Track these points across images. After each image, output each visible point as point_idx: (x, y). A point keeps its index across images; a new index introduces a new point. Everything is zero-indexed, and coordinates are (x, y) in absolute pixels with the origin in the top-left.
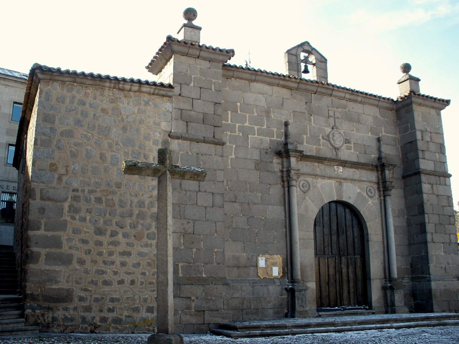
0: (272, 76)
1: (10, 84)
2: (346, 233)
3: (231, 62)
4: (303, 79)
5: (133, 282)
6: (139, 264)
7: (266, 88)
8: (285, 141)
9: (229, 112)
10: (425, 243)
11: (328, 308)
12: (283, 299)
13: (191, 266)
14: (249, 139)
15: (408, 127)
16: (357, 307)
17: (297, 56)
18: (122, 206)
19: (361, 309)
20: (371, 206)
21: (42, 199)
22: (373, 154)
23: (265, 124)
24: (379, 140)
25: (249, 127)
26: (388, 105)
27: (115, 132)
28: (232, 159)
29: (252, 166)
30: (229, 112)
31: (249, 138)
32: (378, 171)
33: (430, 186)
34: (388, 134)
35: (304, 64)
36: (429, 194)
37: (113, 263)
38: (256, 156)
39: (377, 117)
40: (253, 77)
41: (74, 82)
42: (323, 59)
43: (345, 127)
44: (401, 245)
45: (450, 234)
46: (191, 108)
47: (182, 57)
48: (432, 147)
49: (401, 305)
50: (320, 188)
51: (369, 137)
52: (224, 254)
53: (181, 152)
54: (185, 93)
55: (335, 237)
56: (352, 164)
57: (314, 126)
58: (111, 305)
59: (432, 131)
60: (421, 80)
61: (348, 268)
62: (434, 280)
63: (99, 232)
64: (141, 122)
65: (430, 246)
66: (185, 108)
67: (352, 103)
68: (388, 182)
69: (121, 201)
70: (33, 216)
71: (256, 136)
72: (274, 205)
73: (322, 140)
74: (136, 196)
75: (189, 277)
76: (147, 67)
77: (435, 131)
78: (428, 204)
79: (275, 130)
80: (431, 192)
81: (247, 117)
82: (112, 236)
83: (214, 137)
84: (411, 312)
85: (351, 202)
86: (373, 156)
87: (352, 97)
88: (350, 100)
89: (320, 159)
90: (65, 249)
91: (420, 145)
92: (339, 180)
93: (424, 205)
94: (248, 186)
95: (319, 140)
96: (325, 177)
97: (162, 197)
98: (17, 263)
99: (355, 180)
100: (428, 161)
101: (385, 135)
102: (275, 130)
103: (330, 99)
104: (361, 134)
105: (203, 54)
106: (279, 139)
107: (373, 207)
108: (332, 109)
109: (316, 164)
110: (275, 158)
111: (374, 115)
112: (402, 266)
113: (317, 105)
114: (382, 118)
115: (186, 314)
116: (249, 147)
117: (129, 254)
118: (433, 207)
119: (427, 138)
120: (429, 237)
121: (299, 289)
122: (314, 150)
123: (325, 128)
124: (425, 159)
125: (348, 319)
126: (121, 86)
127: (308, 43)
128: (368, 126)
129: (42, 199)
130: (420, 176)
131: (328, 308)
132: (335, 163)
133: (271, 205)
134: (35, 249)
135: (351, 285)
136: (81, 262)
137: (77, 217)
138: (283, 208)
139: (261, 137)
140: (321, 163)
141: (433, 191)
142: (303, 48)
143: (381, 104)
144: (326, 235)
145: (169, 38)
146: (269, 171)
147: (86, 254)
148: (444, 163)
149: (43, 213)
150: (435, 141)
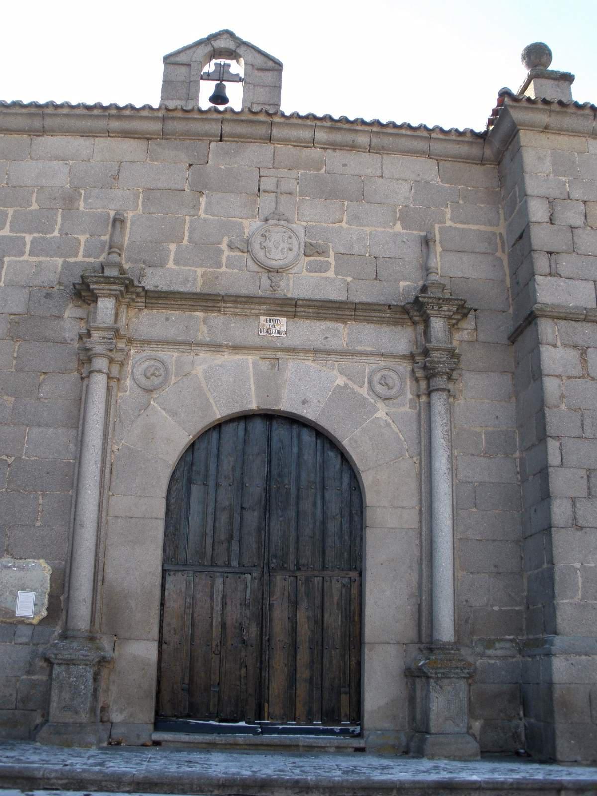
0: (85, 112)
2: (297, 504)
11: (211, 722)
14: (5, 267)
16: (318, 725)
19: (332, 732)
20: (382, 423)
22: (405, 279)
23: (57, 227)
24: (427, 242)
25: (11, 238)
26: (464, 149)
31: (6, 263)
32: (415, 324)
34: (464, 223)
36: (569, 377)
38: (45, 294)
40: (37, 123)
43: (310, 215)
44: (494, 541)
49: (457, 729)
50: (201, 375)
51: (395, 235)
55: (256, 514)
56: (319, 308)
57: (205, 220)
60: (521, 50)
61: (295, 605)
62: (566, 652)
65: (560, 538)
67: (342, 152)
68: (438, 350)
72: (47, 426)
73: (227, 252)
78: (563, 407)
79: (82, 238)
81: (10, 216)
85: (310, 413)
86: (403, 284)
87: (338, 137)
88: (334, 146)
89: (207, 300)
93: (547, 411)
95: (221, 252)
96: (221, 346)
99: (329, 352)
100: (570, 281)
101: (456, 228)
102: (82, 238)
103: (269, 148)
104: (367, 229)
106: (92, 260)
107: (393, 426)
108: (272, 172)
109: (200, 315)
110: (70, 306)
111: (418, 179)
112: (492, 606)
113: (223, 167)
114: (447, 185)
118: (582, 416)
120: (560, 511)
121: (60, 657)
122: (199, 278)
123: (244, 221)
124: (561, 276)
128: (395, 206)
131: (211, 722)
132: (257, 307)
133: (39, 425)
135: (303, 656)
139: (41, 259)
140: (213, 311)
142: (213, 46)
143: (437, 147)
144: (224, 509)
146: (47, 340)
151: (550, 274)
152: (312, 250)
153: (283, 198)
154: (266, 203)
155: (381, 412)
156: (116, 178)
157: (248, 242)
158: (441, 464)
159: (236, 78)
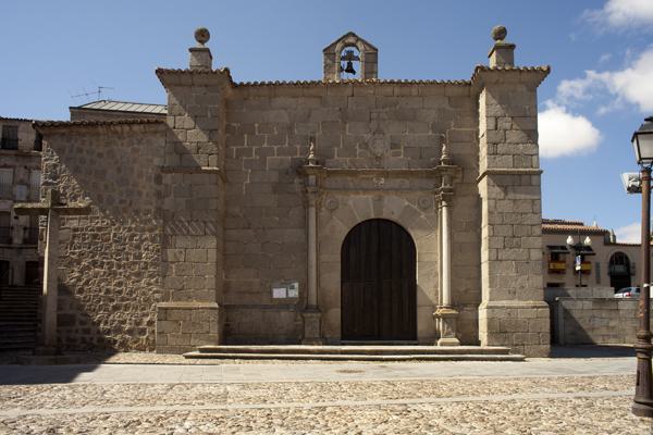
9: (246, 136)
38: (274, 177)
64: (135, 161)
75: (611, 319)
79: (298, 147)
85: (394, 218)
102: (298, 147)
104: (417, 135)
152: (394, 146)
154: (373, 125)
156: (309, 116)
159: (357, 59)
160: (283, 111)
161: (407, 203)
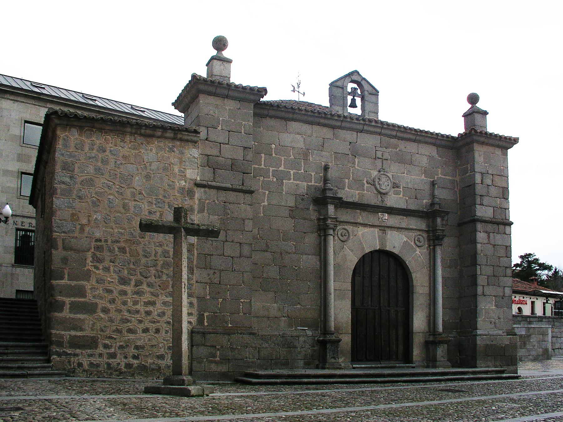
1: (19, 99)
3: (265, 99)
4: (348, 114)
5: (157, 331)
6: (164, 313)
7: (306, 128)
8: (324, 187)
9: (263, 155)
10: (475, 296)
12: (315, 351)
13: (217, 316)
15: (467, 168)
17: (343, 88)
18: (146, 256)
21: (65, 248)
24: (433, 184)
27: (138, 182)
28: (264, 206)
29: (287, 213)
30: (263, 155)
33: (486, 235)
35: (352, 97)
37: (138, 312)
38: (291, 203)
39: (433, 157)
41: (92, 128)
42: (374, 90)
43: (394, 169)
45: (504, 287)
46: (218, 154)
47: (209, 97)
48: (493, 191)
51: (423, 180)
52: (251, 305)
53: (207, 201)
54: (212, 137)
58: (136, 352)
59: (495, 173)
63: (124, 281)
65: (480, 299)
66: (212, 154)
69: (145, 251)
70: (56, 264)
71: (292, 181)
73: (366, 185)
74: (161, 246)
76: (173, 104)
77: (498, 173)
80: (486, 241)
82: (136, 286)
83: (243, 184)
84: (453, 367)
85: (396, 251)
86: (424, 201)
90: (89, 298)
91: (479, 189)
92: (382, 228)
94: (282, 235)
97: (177, 253)
98: (39, 310)
99: (402, 228)
102: (313, 174)
104: (413, 177)
105: (231, 93)
106: (317, 184)
108: (380, 149)
115: (211, 362)
116: (284, 193)
117: (153, 303)
119: (488, 181)
120: (480, 290)
125: (358, 366)
126: (143, 131)
127: (358, 73)
129: (65, 248)
130: (475, 224)
134: (59, 298)
136: (105, 310)
137: (101, 267)
138: (318, 257)
139: (298, 182)
141: (489, 240)
145: (194, 76)
147: (110, 303)
148: (505, 209)
149: (66, 264)
150: (497, 185)
151: (480, 205)
153: (384, 161)
155: (418, 251)
157: (374, 181)
158: (439, 272)
160: (299, 137)
161: (405, 239)
